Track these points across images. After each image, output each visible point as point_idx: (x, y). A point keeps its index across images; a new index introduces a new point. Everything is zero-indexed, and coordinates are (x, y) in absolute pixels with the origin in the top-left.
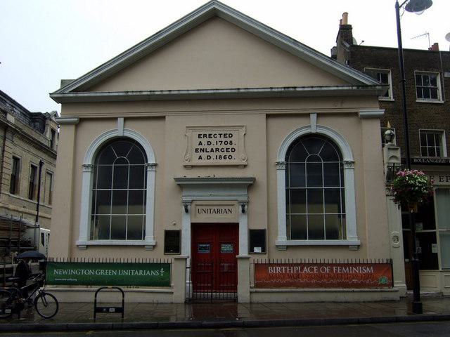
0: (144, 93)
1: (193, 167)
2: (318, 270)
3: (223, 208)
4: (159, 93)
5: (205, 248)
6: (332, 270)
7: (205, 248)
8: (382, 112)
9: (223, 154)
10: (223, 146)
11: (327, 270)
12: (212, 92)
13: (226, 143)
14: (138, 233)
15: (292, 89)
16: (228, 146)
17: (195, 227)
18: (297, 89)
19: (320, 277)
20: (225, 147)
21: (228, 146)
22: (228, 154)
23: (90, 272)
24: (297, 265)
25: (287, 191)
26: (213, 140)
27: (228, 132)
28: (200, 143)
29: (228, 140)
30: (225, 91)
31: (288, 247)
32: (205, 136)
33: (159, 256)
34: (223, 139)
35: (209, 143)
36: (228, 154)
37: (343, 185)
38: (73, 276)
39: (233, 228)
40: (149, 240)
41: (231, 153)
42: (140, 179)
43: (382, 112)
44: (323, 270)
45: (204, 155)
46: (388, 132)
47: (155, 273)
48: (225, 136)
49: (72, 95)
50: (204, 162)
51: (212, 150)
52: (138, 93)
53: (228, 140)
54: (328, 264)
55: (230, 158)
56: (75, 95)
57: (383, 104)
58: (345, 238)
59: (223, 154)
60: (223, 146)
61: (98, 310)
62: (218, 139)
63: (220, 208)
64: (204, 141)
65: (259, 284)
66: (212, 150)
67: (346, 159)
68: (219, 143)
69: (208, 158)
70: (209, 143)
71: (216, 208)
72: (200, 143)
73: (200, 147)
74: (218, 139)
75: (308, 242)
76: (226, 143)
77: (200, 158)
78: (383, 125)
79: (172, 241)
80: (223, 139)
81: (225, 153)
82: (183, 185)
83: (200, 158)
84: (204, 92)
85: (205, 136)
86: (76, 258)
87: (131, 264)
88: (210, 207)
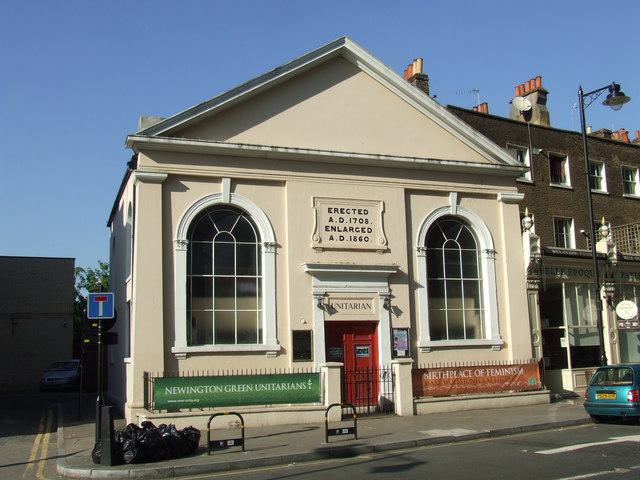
0: (263, 149)
1: (324, 249)
2: (473, 374)
3: (362, 302)
4: (283, 150)
5: (364, 351)
6: (485, 374)
7: (364, 351)
8: (521, 196)
9: (358, 235)
10: (358, 224)
11: (481, 372)
12: (348, 155)
13: (361, 222)
14: (249, 335)
15: (436, 162)
16: (364, 225)
17: (328, 325)
18: (442, 163)
19: (475, 381)
20: (360, 226)
21: (364, 225)
22: (364, 235)
23: (216, 388)
24: (451, 369)
25: (188, 279)
26: (346, 217)
27: (363, 208)
28: (331, 220)
29: (364, 217)
30: (345, 155)
31: (433, 349)
32: (336, 210)
33: (288, 364)
34: (358, 217)
35: (341, 220)
36: (364, 235)
37: (260, 274)
38: (194, 396)
39: (370, 327)
40: (268, 341)
41: (366, 234)
42: (471, 269)
43: (521, 196)
44: (477, 372)
45: (336, 235)
46: (527, 219)
47: (301, 386)
48: (360, 213)
49: (162, 141)
50: (337, 244)
51: (345, 230)
52: (256, 148)
53: (364, 217)
54: (482, 367)
55: (367, 239)
56: (166, 141)
57: (522, 186)
58: (261, 342)
59: (358, 235)
60: (358, 224)
61: (330, 432)
62: (352, 215)
63: (357, 302)
64: (336, 216)
65: (418, 391)
66: (345, 230)
67: (263, 240)
68: (353, 221)
69: (342, 238)
70: (341, 220)
71: (353, 302)
72: (331, 220)
73: (331, 224)
74: (352, 215)
75: (236, 347)
76: (361, 220)
77: (331, 238)
78: (522, 210)
79: (302, 344)
80: (358, 217)
81: (361, 234)
82: (321, 272)
83: (331, 238)
84: (339, 155)
85: (336, 210)
86: (235, 371)
87: (213, 377)
88: (346, 301)
